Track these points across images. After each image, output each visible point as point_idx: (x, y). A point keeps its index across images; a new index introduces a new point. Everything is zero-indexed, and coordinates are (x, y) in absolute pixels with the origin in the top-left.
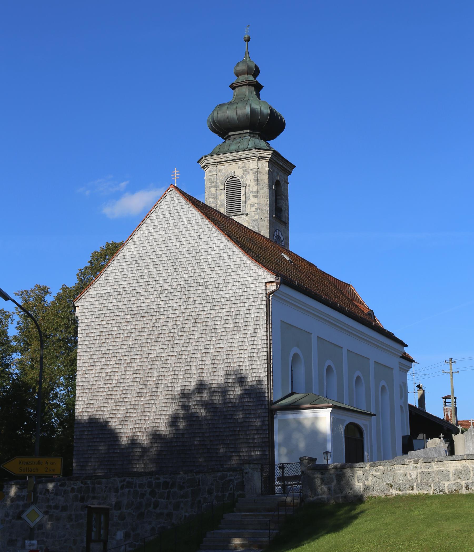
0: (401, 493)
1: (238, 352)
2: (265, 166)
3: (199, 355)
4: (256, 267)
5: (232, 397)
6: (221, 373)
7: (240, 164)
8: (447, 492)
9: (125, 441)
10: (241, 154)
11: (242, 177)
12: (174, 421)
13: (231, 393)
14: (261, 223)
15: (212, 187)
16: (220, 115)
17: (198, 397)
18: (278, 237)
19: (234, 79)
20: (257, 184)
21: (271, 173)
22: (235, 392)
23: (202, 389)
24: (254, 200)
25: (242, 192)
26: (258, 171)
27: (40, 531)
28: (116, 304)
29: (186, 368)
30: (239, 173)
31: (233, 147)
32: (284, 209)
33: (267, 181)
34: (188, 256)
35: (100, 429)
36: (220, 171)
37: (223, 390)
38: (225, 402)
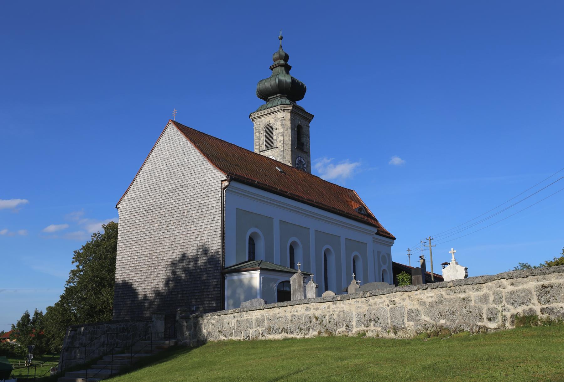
0: (225, 339)
1: (204, 232)
2: (288, 115)
3: (182, 236)
4: (216, 170)
5: (199, 265)
6: (194, 248)
7: (273, 116)
8: (251, 338)
9: (141, 297)
10: (272, 109)
12: (167, 283)
13: (200, 262)
14: (285, 152)
16: (261, 86)
17: (181, 265)
18: (300, 161)
19: (272, 63)
20: (283, 128)
21: (292, 120)
22: (202, 260)
23: (183, 260)
24: (281, 138)
25: (274, 134)
26: (283, 119)
28: (138, 204)
29: (175, 246)
30: (272, 122)
31: (269, 106)
32: (305, 144)
33: (289, 125)
35: (127, 288)
37: (195, 259)
38: (197, 267)
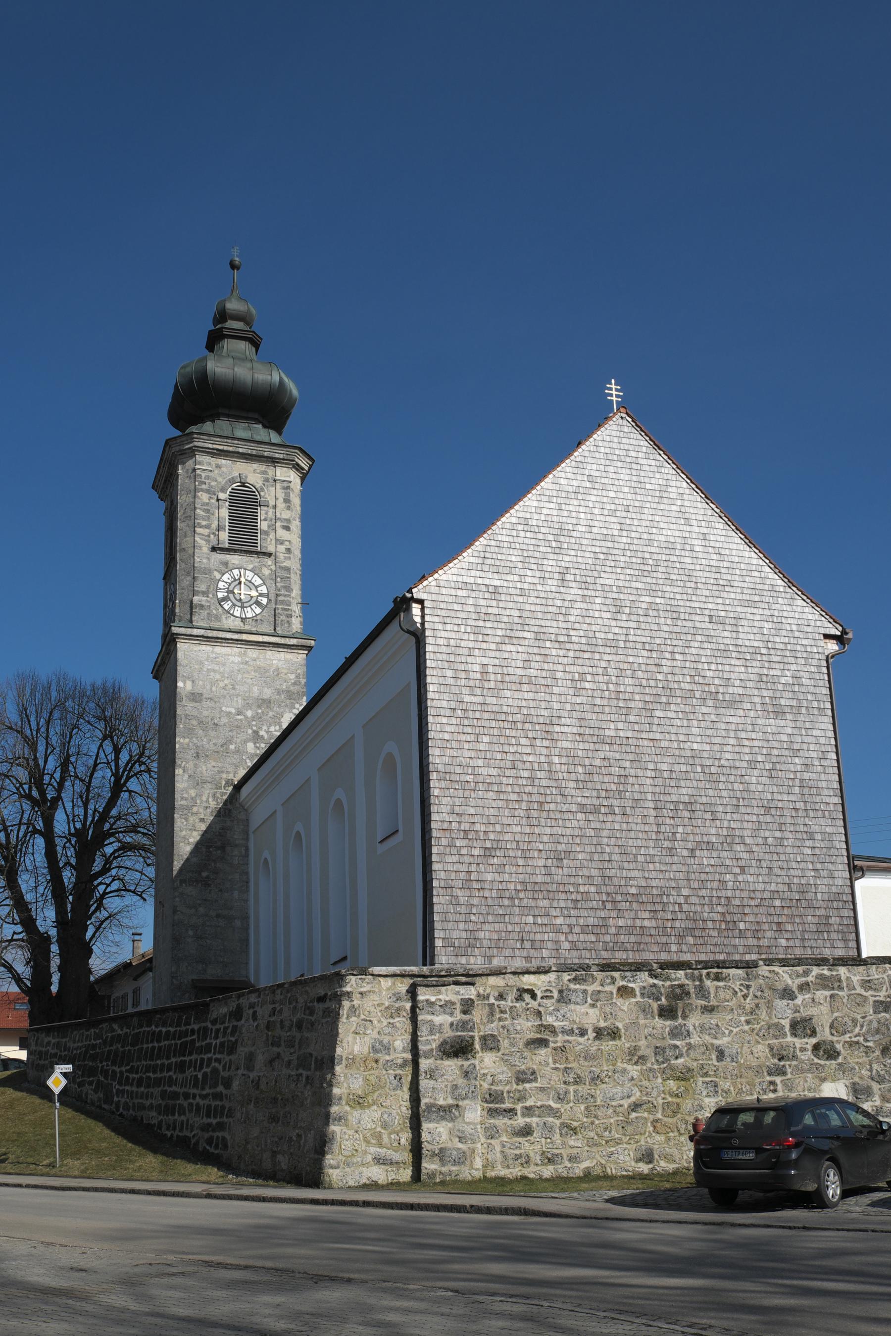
11: (262, 489)
15: (202, 490)
24: (282, 533)
27: (527, 1086)
34: (668, 552)
36: (218, 467)
